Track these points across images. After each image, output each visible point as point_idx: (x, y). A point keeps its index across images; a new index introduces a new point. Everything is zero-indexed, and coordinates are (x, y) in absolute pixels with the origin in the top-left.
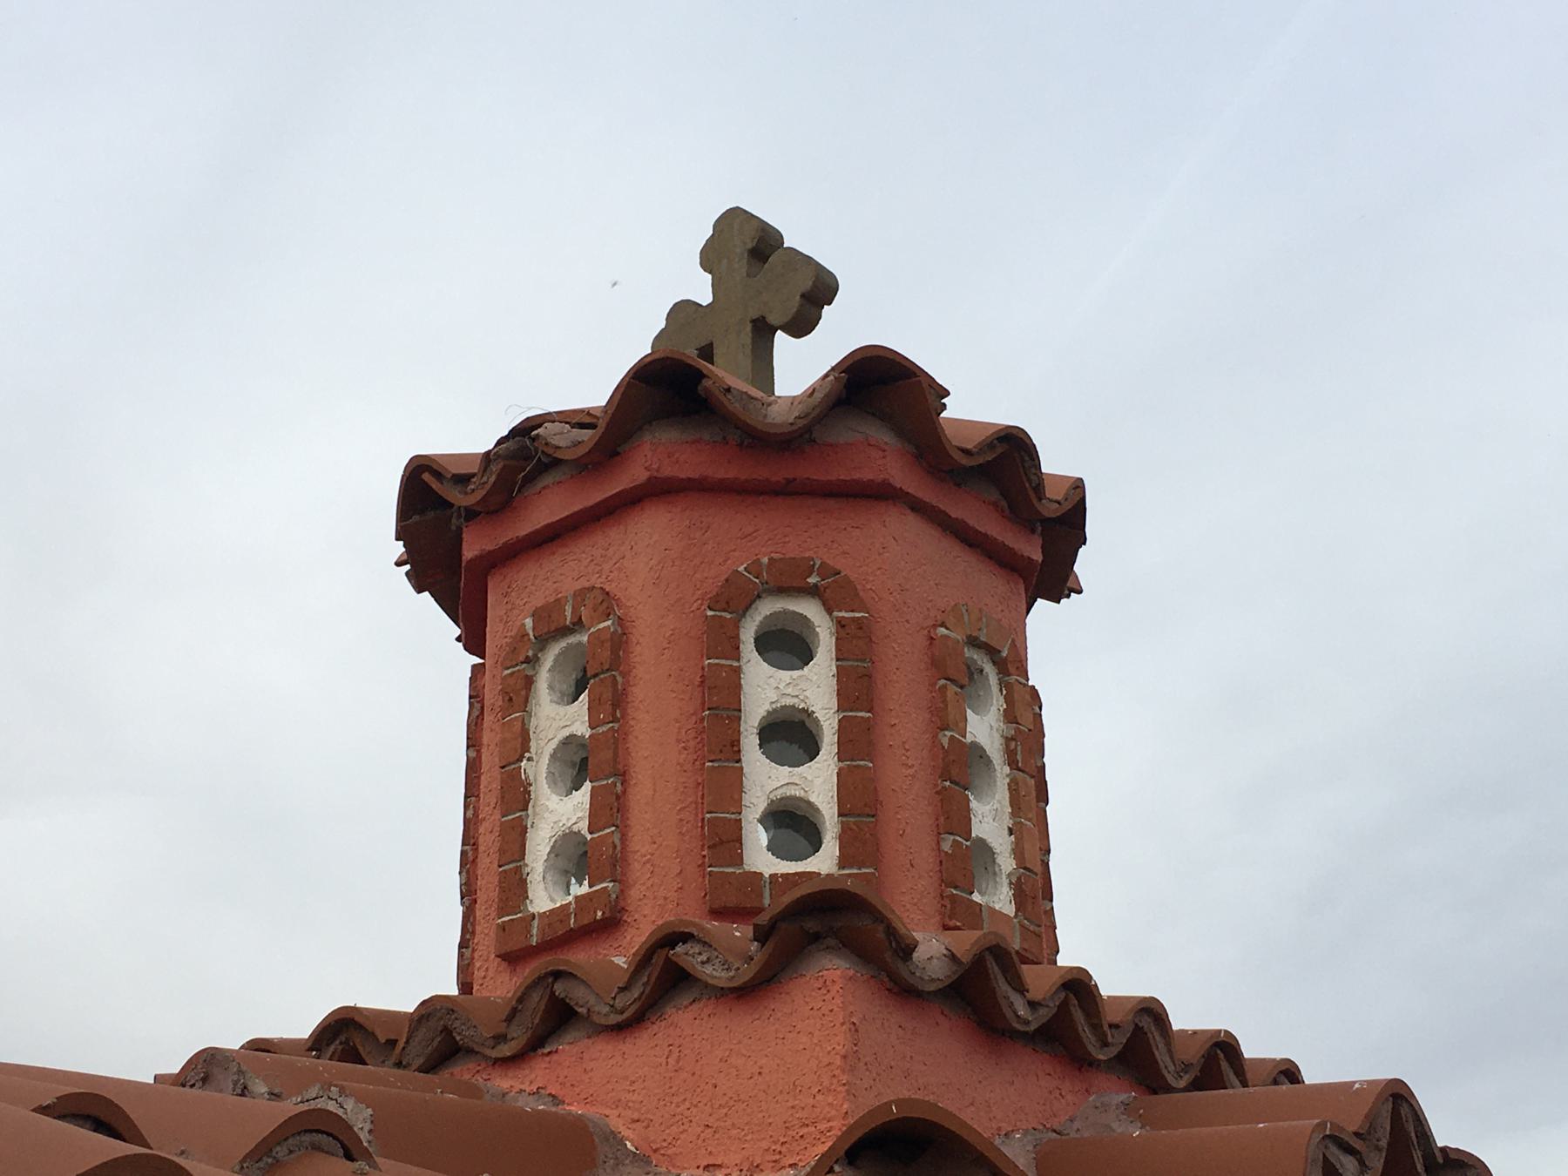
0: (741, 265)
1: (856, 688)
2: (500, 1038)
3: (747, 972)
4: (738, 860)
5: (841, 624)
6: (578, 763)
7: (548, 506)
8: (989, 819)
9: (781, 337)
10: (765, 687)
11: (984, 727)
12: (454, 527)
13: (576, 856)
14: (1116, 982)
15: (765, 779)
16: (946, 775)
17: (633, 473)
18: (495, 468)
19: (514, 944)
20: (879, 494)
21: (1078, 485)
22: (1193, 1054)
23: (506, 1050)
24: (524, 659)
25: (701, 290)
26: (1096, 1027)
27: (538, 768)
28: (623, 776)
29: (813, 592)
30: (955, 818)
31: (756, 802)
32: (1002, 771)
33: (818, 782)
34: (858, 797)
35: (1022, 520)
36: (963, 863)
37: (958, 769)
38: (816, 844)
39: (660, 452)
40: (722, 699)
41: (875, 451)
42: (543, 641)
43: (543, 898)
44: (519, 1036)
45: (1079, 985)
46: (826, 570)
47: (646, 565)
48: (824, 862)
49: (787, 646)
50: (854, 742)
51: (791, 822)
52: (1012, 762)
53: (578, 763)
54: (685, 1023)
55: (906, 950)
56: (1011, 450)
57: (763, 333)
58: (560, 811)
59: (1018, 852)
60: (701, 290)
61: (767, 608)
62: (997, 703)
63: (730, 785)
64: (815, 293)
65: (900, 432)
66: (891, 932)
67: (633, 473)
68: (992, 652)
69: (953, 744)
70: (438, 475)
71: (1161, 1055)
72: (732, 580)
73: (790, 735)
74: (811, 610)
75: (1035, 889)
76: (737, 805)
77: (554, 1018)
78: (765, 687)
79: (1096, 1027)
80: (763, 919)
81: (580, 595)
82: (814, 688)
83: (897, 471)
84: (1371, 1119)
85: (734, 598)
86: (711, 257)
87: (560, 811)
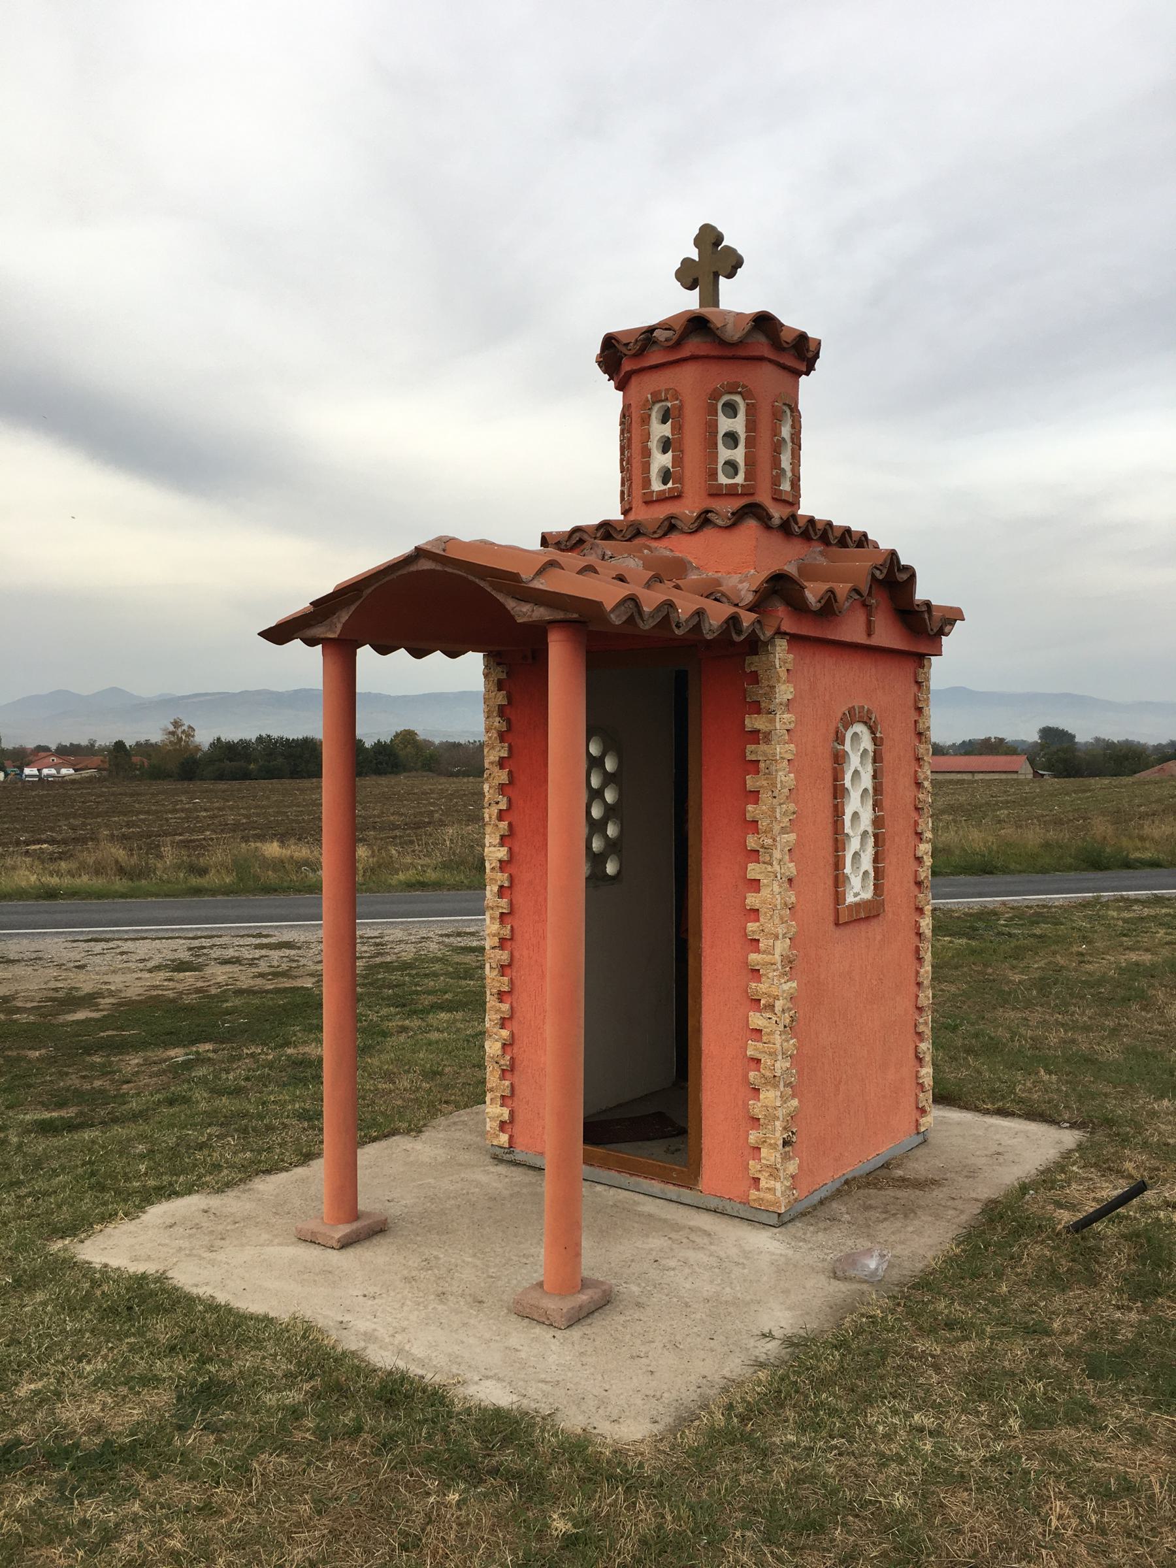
0: (709, 248)
1: (751, 426)
2: (655, 532)
3: (729, 523)
4: (716, 480)
5: (748, 405)
7: (655, 358)
8: (785, 461)
9: (722, 279)
10: (725, 424)
11: (786, 432)
12: (619, 356)
13: (666, 476)
14: (820, 515)
15: (724, 454)
16: (775, 451)
17: (686, 352)
18: (639, 344)
19: (648, 499)
20: (761, 359)
21: (819, 343)
22: (838, 534)
23: (656, 536)
24: (647, 407)
25: (694, 254)
26: (814, 531)
27: (654, 445)
28: (682, 451)
29: (740, 393)
31: (722, 431)
32: (790, 444)
33: (739, 455)
34: (750, 460)
35: (801, 353)
37: (777, 448)
38: (736, 473)
39: (694, 345)
40: (712, 427)
42: (654, 403)
43: (657, 486)
44: (660, 532)
46: (744, 386)
47: (688, 382)
48: (740, 479)
50: (750, 443)
51: (732, 465)
52: (793, 442)
54: (708, 533)
55: (770, 518)
56: (803, 337)
57: (716, 276)
58: (661, 460)
59: (793, 470)
60: (694, 254)
61: (725, 398)
62: (790, 422)
63: (714, 456)
64: (732, 263)
65: (767, 336)
66: (768, 514)
67: (686, 352)
68: (789, 406)
69: (776, 433)
70: (618, 341)
71: (831, 536)
72: (715, 390)
73: (732, 439)
74: (738, 399)
76: (716, 463)
78: (725, 424)
79: (814, 531)
81: (667, 390)
82: (738, 424)
83: (767, 352)
84: (885, 561)
85: (715, 396)
86: (698, 242)
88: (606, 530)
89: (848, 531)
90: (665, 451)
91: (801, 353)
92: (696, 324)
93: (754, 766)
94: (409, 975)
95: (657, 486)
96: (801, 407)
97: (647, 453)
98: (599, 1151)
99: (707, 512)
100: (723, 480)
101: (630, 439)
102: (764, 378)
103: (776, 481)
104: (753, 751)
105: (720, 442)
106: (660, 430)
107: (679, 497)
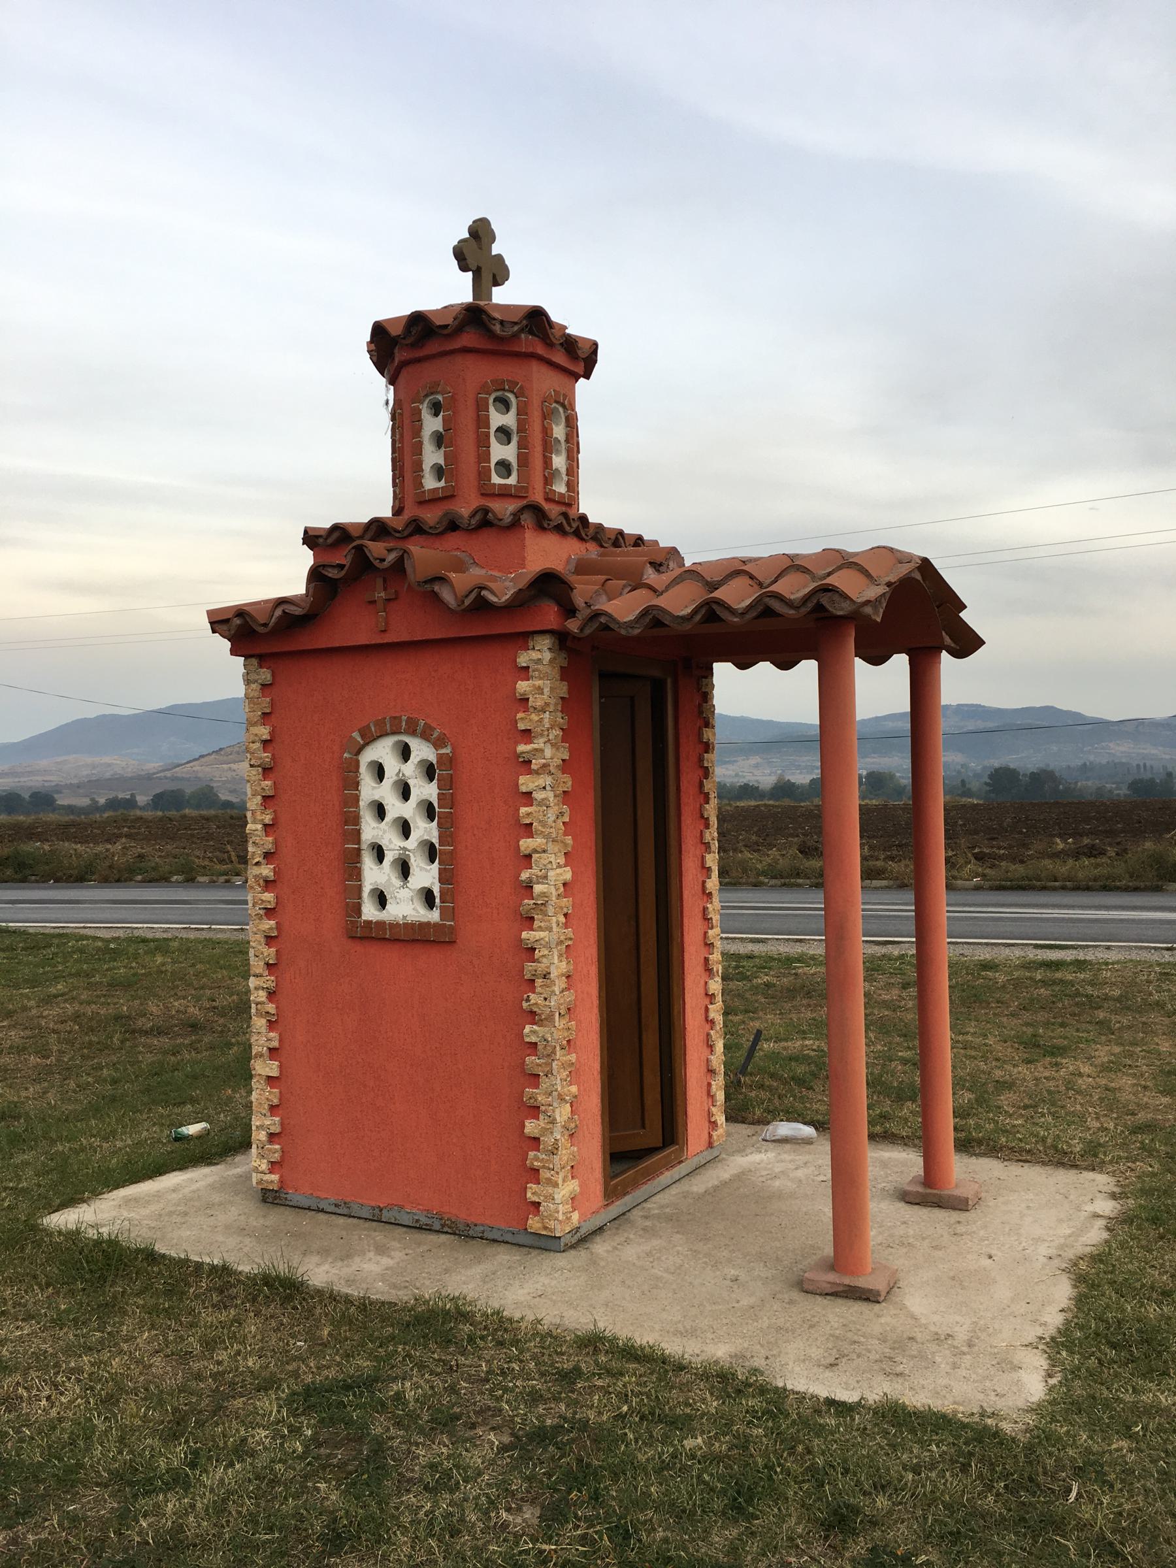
6: (439, 440)
8: (559, 462)
10: (497, 419)
11: (559, 431)
13: (439, 472)
30: (547, 462)
31: (494, 459)
35: (580, 357)
36: (549, 477)
37: (548, 445)
38: (509, 475)
41: (529, 343)
43: (430, 483)
45: (583, 519)
48: (512, 480)
49: (504, 405)
53: (439, 440)
69: (551, 431)
74: (511, 396)
75: (572, 486)
77: (417, 528)
78: (497, 419)
80: (564, 509)
87: (432, 456)
88: (377, 528)
89: (621, 533)
90: (436, 415)
91: (580, 357)
92: (474, 316)
93: (534, 1174)
94: (349, 1423)
95: (430, 483)
96: (579, 408)
97: (418, 449)
98: (235, 812)
99: (482, 588)
100: (496, 479)
101: (402, 467)
102: (543, 381)
103: (548, 480)
104: (534, 1158)
105: (493, 439)
106: (432, 424)
107: (453, 496)
